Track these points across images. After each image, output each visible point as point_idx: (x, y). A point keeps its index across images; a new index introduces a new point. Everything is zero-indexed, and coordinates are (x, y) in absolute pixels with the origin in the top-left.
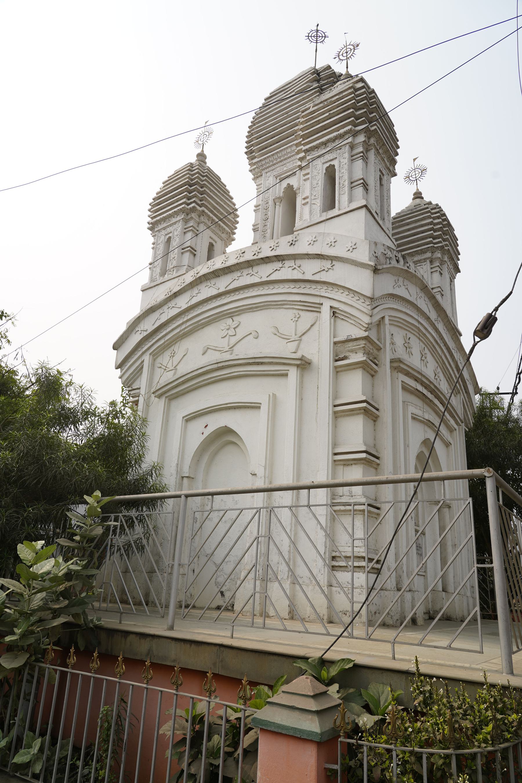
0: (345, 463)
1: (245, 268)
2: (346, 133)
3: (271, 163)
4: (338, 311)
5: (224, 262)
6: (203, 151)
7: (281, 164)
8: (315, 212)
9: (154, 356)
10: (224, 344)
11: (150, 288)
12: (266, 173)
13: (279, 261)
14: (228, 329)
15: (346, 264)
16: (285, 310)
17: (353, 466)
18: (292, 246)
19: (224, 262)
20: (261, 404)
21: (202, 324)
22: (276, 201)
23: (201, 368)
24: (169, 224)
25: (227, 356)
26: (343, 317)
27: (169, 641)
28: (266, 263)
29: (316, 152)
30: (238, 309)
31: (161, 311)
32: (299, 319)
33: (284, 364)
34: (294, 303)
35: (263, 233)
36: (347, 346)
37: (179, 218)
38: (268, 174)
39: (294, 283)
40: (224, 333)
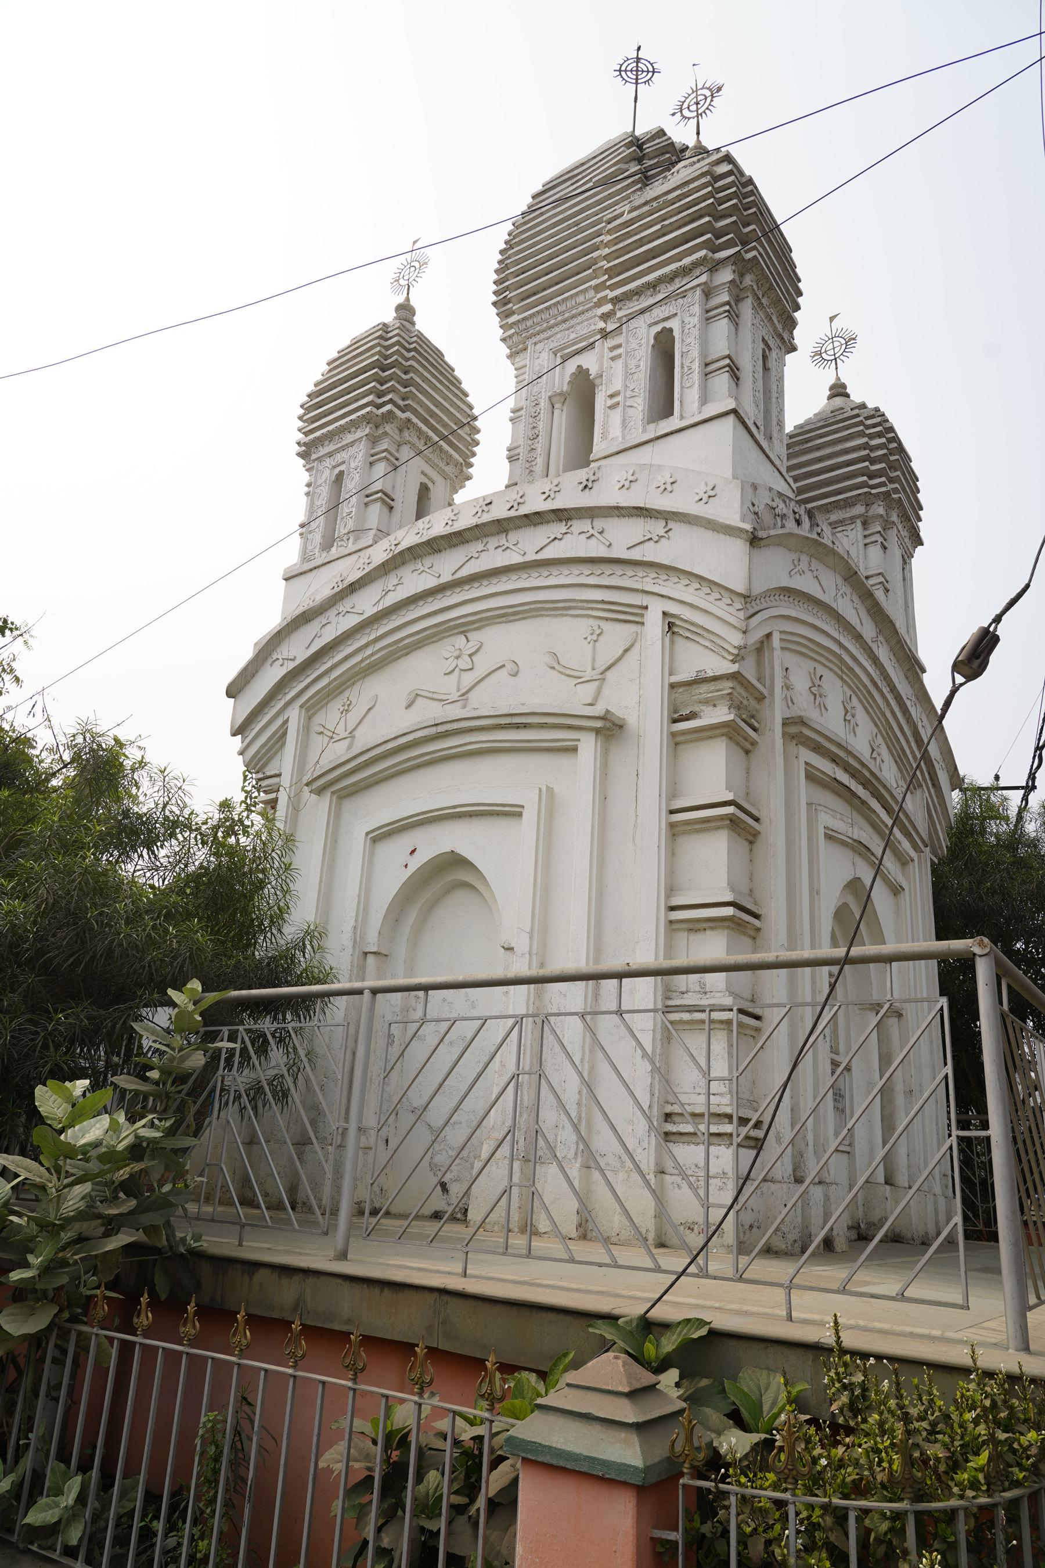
0: (691, 926)
1: (492, 535)
2: (695, 264)
3: (545, 325)
4: (678, 622)
5: (450, 523)
6: (408, 299)
7: (564, 326)
8: (632, 423)
9: (308, 710)
11: (301, 574)
12: (535, 344)
13: (561, 520)
14: (457, 658)
15: (695, 528)
17: (708, 932)
18: (587, 490)
19: (450, 523)
20: (523, 807)
21: (406, 647)
22: (554, 400)
23: (404, 734)
24: (340, 445)
25: (455, 712)
27: (339, 1281)
28: (535, 525)
29: (636, 303)
30: (479, 617)
31: (322, 620)
32: (601, 638)
33: (570, 727)
34: (590, 605)
35: (528, 465)
38: (538, 346)
39: (590, 566)
40: (450, 664)
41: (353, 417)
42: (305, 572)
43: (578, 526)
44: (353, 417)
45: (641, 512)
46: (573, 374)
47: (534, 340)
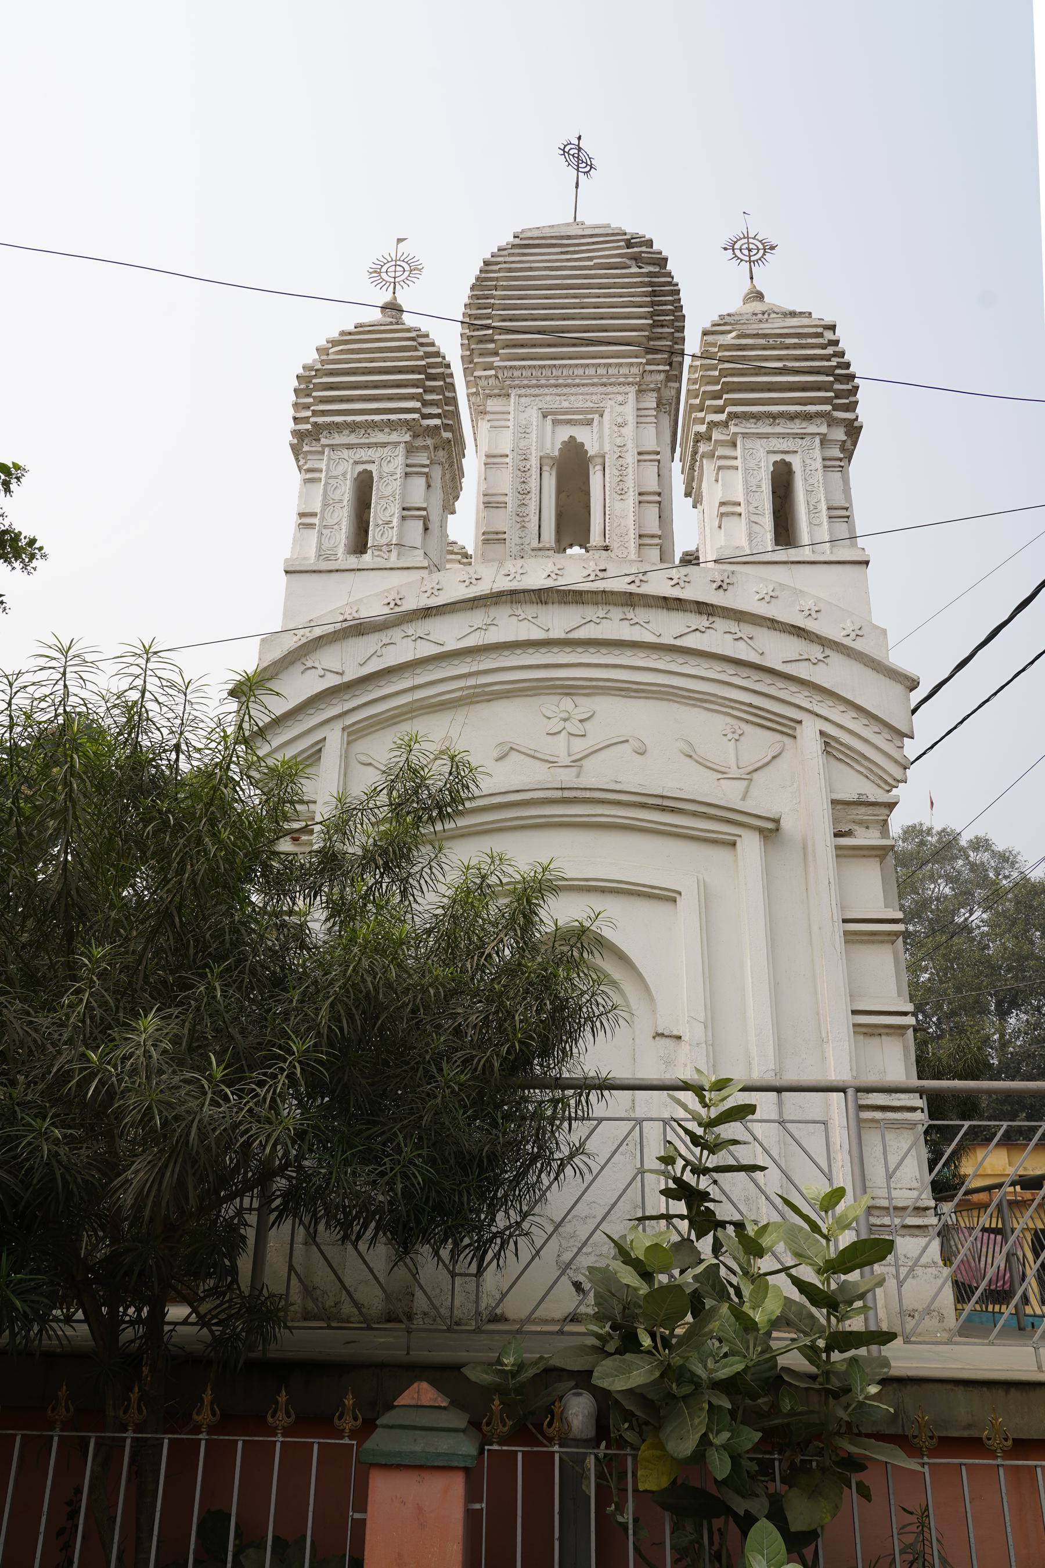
0: (870, 1030)
1: (615, 605)
2: (819, 415)
3: (534, 382)
4: (833, 744)
5: (553, 576)
6: (395, 298)
7: (555, 391)
9: (349, 734)
10: (558, 747)
11: (314, 572)
12: (520, 396)
13: (700, 613)
14: (565, 720)
15: (853, 662)
16: (706, 712)
17: (884, 1038)
18: (721, 591)
19: (553, 576)
20: (680, 893)
22: (545, 461)
23: (518, 791)
24: (363, 441)
25: (567, 777)
26: (841, 756)
27: (949, 1387)
28: (668, 609)
29: (753, 426)
30: (594, 683)
31: (384, 637)
32: (742, 738)
34: (732, 704)
36: (855, 812)
37: (394, 437)
38: (523, 400)
39: (733, 666)
40: (555, 725)
41: (393, 417)
42: (320, 572)
43: (721, 624)
44: (393, 417)
45: (798, 632)
46: (564, 442)
47: (523, 391)
